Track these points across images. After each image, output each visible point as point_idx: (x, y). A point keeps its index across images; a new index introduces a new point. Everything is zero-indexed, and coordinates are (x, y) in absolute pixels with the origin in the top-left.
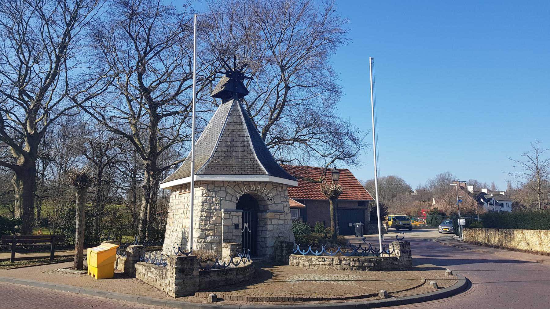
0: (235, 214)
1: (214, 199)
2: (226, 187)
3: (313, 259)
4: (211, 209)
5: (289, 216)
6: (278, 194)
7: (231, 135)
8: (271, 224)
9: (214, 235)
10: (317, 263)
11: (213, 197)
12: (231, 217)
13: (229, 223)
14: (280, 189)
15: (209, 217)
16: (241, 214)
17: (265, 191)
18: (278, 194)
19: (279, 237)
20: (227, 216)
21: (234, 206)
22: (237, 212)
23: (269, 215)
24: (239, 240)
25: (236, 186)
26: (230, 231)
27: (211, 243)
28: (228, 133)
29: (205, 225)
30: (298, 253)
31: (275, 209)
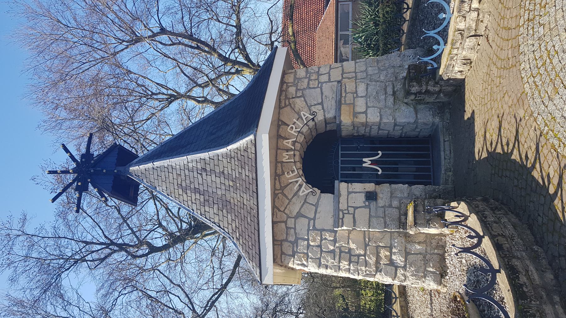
0: (343, 199)
1: (312, 244)
2: (288, 217)
3: (462, 26)
4: (333, 252)
5: (349, 65)
6: (303, 96)
7: (189, 192)
8: (365, 113)
9: (390, 248)
10: (474, 14)
11: (309, 245)
12: (351, 210)
13: (362, 214)
14: (292, 90)
15: (351, 255)
16: (343, 185)
17: (297, 130)
18: (303, 96)
19: (394, 93)
20: (348, 219)
21: (327, 198)
22: (339, 195)
23: (346, 119)
24: (402, 191)
25: (286, 192)
26: (380, 212)
27: (407, 254)
28: (185, 195)
29: (366, 264)
30: (438, 60)
31: (333, 102)
